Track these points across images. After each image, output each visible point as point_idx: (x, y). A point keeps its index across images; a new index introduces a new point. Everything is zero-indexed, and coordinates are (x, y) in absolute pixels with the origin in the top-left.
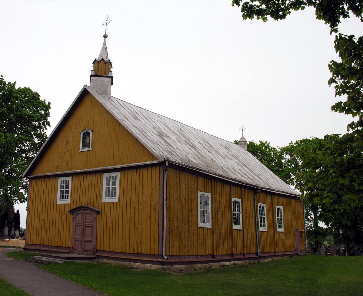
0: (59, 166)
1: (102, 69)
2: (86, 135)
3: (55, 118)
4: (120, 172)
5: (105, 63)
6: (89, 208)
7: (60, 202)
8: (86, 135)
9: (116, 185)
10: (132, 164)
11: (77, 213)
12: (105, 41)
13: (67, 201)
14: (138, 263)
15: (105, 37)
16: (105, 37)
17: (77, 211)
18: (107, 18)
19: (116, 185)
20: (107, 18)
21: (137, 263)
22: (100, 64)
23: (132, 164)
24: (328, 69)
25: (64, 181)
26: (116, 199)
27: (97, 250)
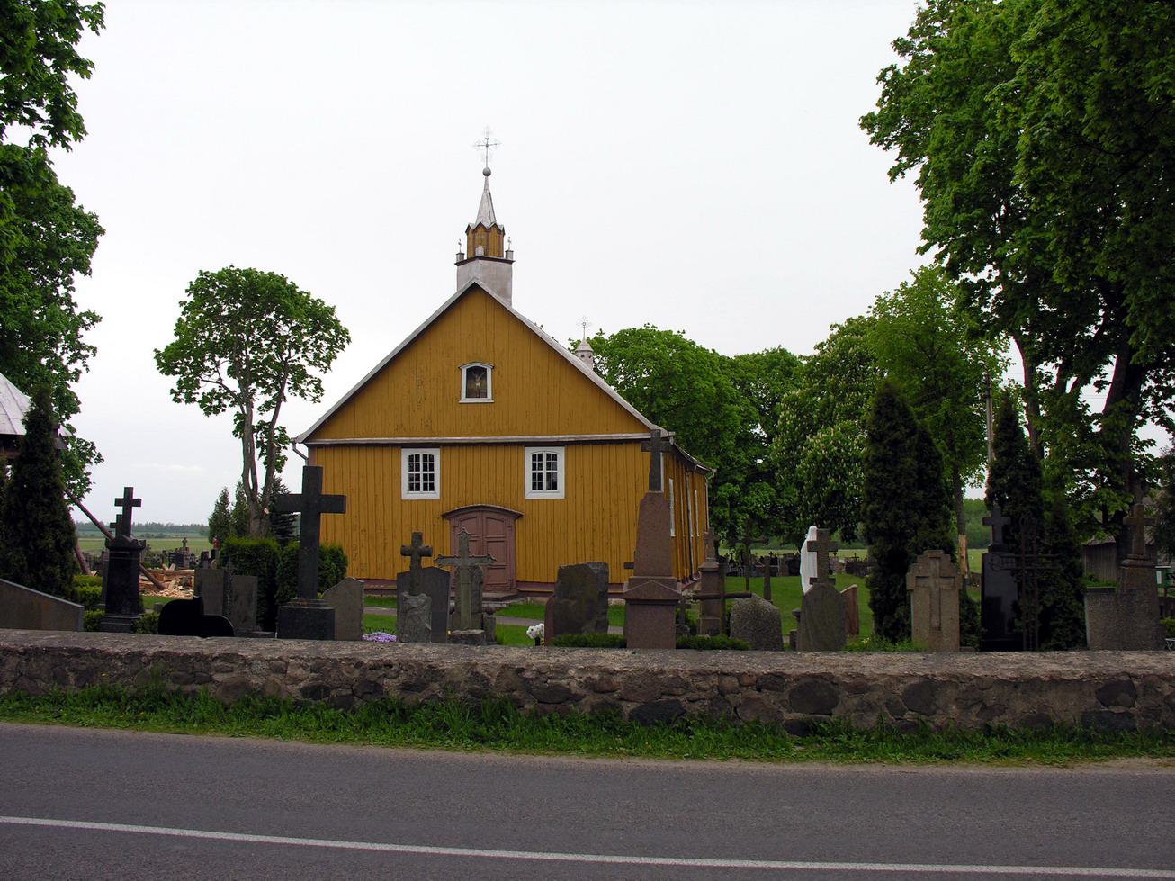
0: (402, 425)
1: (486, 242)
2: (476, 373)
3: (1174, 419)
4: (564, 448)
5: (487, 231)
6: (489, 507)
7: (408, 495)
8: (476, 373)
9: (410, 475)
10: (510, 437)
11: (463, 517)
12: (486, 184)
13: (434, 495)
14: (617, 600)
15: (487, 174)
16: (487, 174)
17: (463, 514)
18: (487, 133)
19: (410, 475)
20: (487, 133)
21: (613, 600)
22: (490, 234)
23: (510, 437)
24: (87, 125)
25: (417, 456)
26: (560, 493)
27: (518, 582)
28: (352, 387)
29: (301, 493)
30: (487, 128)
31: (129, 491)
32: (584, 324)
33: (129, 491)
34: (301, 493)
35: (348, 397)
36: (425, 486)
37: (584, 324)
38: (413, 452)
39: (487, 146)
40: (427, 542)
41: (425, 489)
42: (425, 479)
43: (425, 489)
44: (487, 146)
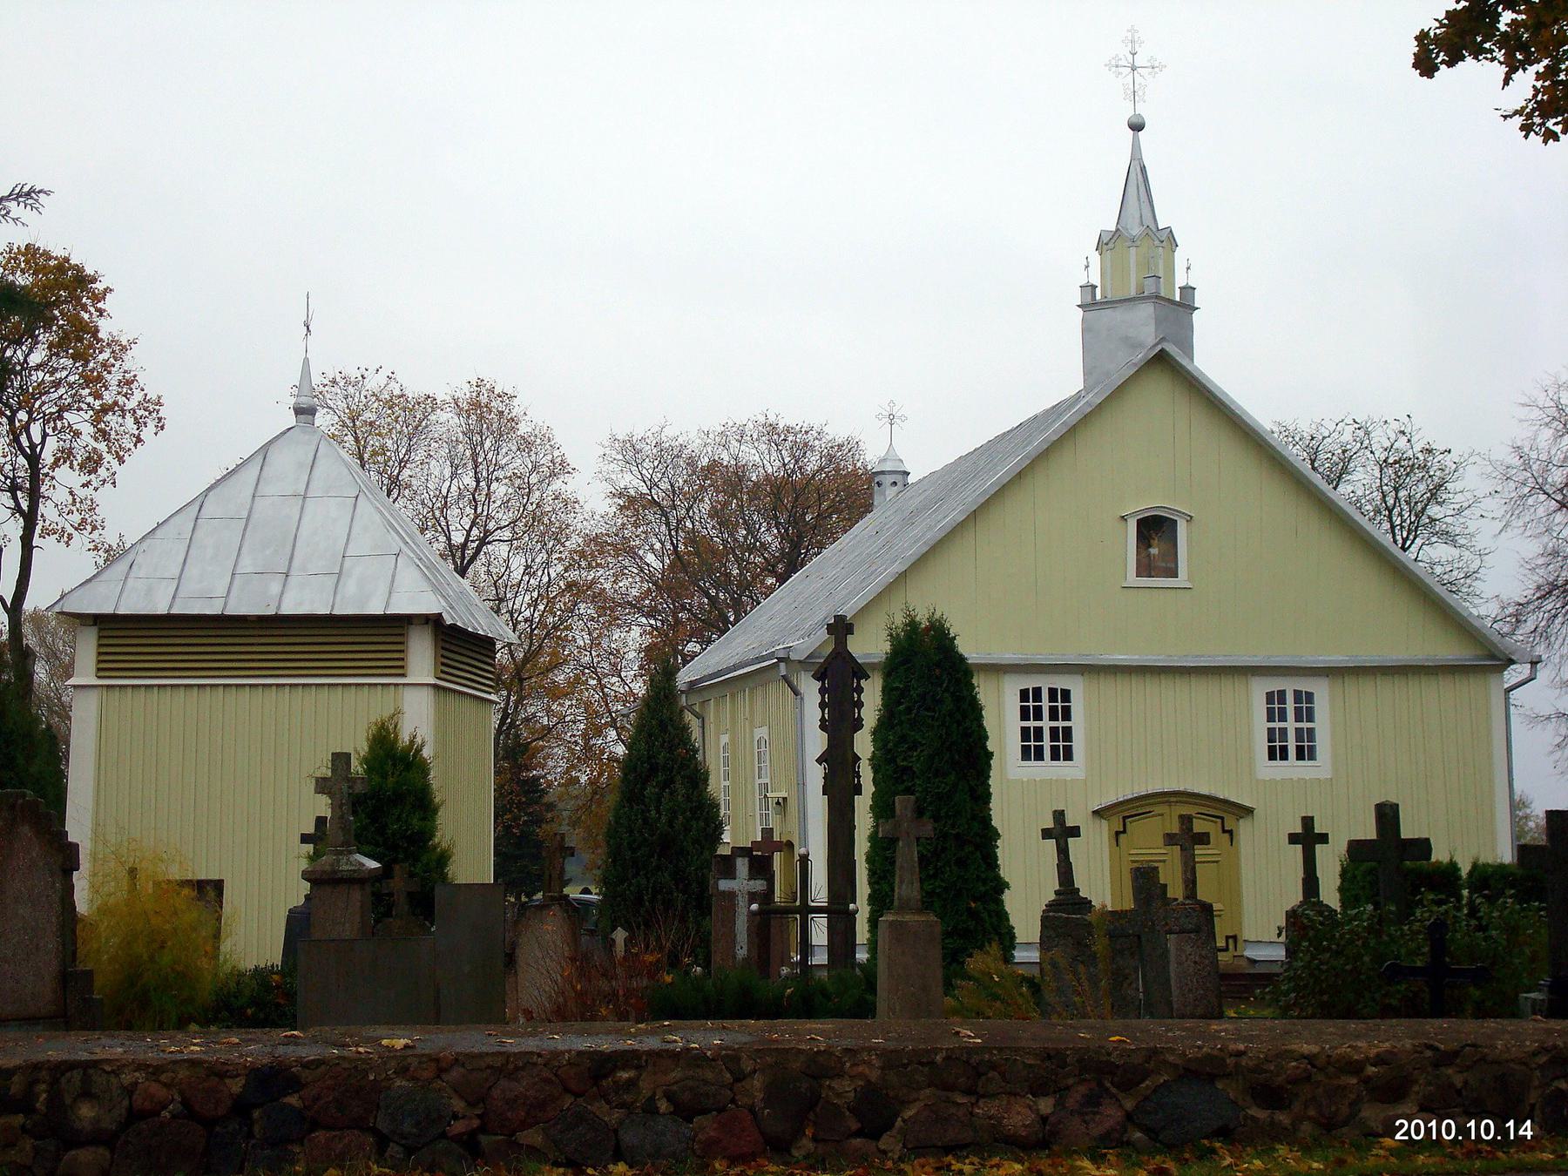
15: (1137, 127)
16: (1137, 127)
25: (1282, 693)
28: (1240, 407)
29: (1374, 837)
30: (1133, 30)
31: (1308, 822)
32: (891, 417)
33: (1308, 822)
34: (1374, 837)
35: (1239, 417)
36: (1055, 750)
37: (891, 417)
38: (1275, 685)
39: (1134, 69)
40: (1244, 828)
41: (1055, 757)
42: (1038, 710)
43: (1055, 757)
44: (1134, 69)
